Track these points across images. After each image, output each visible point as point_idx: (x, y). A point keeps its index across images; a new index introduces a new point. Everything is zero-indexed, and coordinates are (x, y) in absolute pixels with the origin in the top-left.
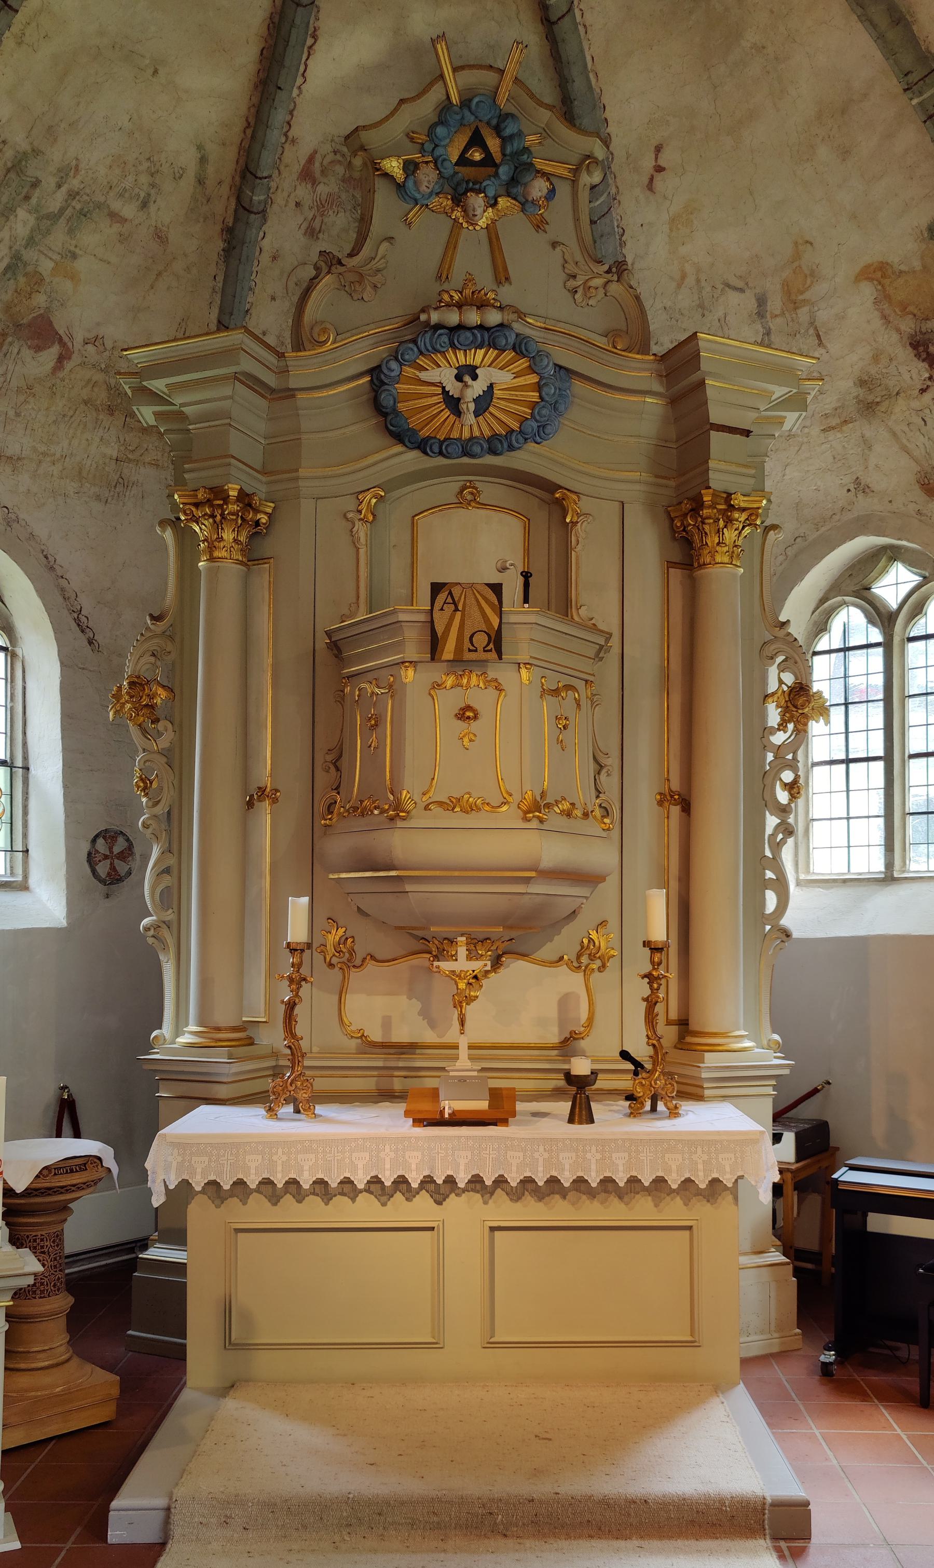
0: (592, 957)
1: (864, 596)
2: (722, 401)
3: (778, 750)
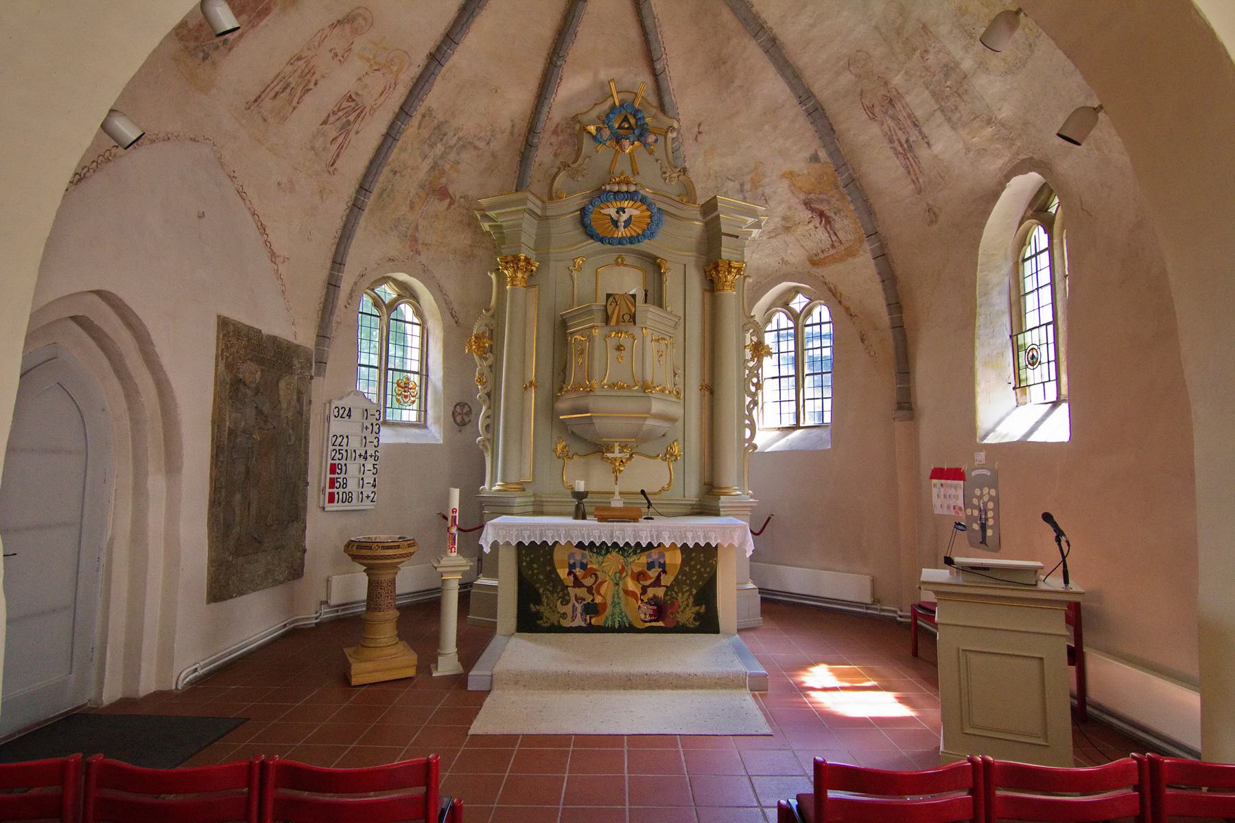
3: (751, 369)
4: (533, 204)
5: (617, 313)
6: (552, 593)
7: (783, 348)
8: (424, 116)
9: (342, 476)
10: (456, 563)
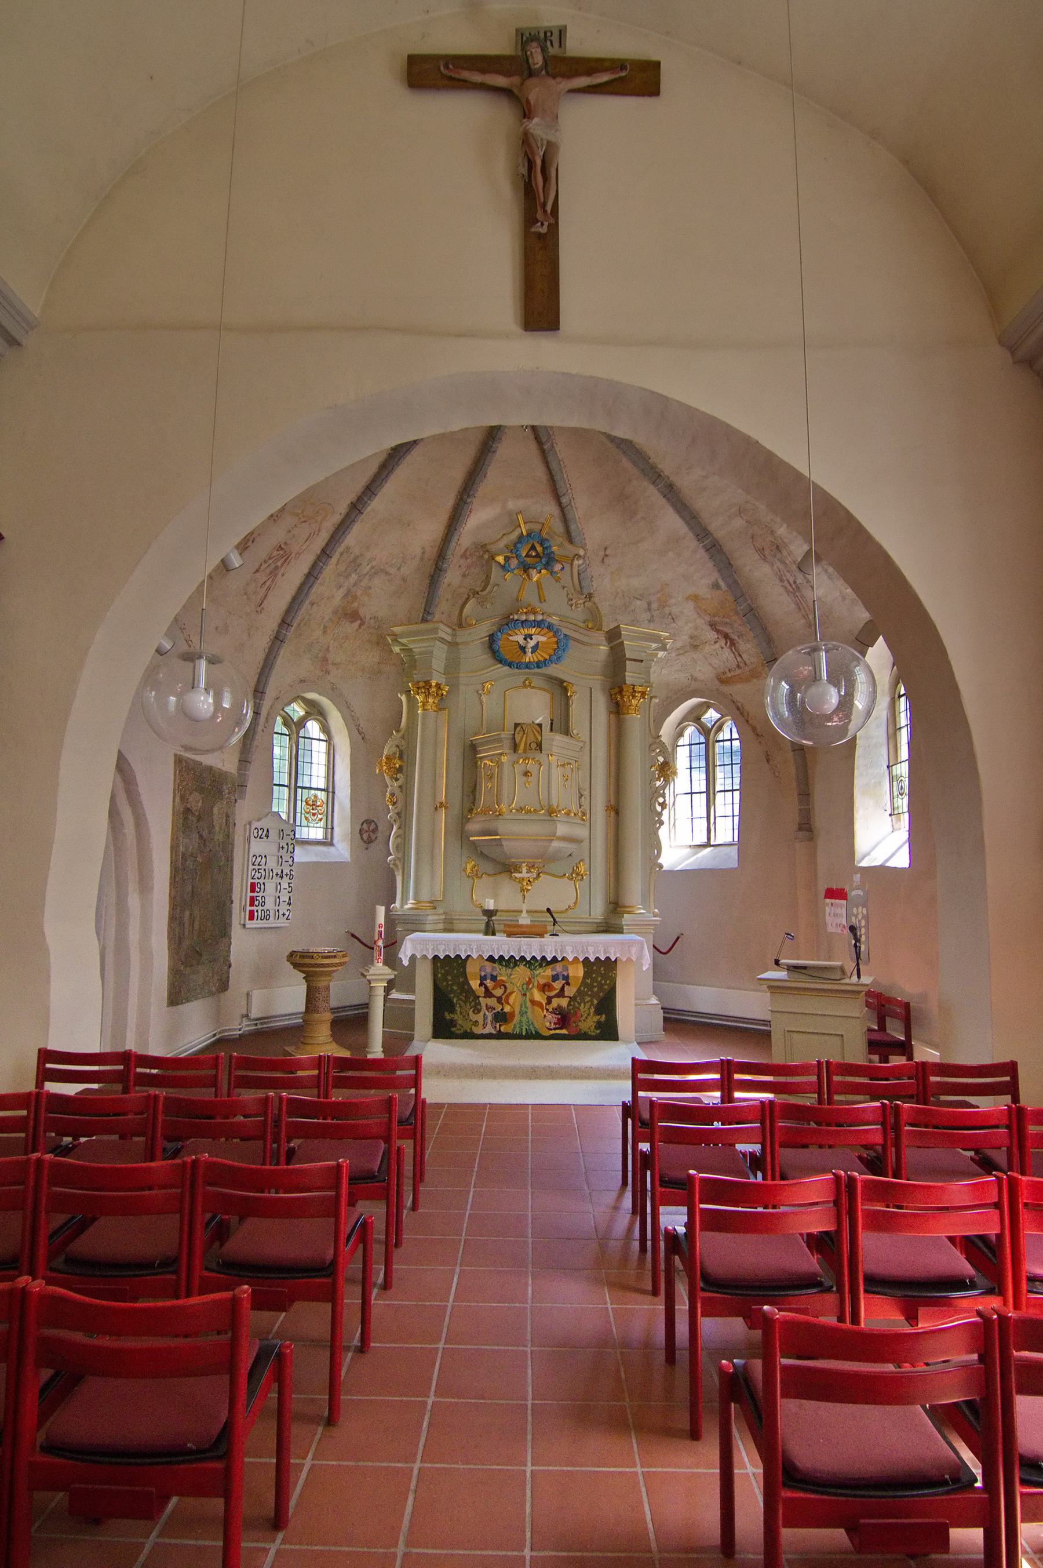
0: (578, 874)
1: (697, 720)
2: (631, 647)
4: (444, 632)
5: (525, 741)
6: (465, 1002)
7: (695, 764)
8: (341, 554)
9: (261, 894)
10: (381, 972)
